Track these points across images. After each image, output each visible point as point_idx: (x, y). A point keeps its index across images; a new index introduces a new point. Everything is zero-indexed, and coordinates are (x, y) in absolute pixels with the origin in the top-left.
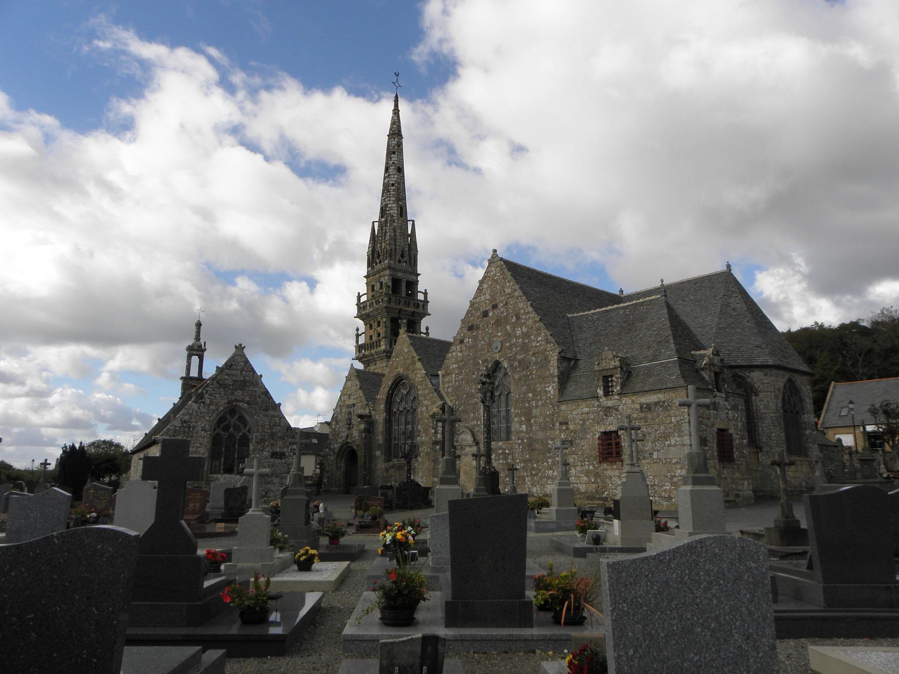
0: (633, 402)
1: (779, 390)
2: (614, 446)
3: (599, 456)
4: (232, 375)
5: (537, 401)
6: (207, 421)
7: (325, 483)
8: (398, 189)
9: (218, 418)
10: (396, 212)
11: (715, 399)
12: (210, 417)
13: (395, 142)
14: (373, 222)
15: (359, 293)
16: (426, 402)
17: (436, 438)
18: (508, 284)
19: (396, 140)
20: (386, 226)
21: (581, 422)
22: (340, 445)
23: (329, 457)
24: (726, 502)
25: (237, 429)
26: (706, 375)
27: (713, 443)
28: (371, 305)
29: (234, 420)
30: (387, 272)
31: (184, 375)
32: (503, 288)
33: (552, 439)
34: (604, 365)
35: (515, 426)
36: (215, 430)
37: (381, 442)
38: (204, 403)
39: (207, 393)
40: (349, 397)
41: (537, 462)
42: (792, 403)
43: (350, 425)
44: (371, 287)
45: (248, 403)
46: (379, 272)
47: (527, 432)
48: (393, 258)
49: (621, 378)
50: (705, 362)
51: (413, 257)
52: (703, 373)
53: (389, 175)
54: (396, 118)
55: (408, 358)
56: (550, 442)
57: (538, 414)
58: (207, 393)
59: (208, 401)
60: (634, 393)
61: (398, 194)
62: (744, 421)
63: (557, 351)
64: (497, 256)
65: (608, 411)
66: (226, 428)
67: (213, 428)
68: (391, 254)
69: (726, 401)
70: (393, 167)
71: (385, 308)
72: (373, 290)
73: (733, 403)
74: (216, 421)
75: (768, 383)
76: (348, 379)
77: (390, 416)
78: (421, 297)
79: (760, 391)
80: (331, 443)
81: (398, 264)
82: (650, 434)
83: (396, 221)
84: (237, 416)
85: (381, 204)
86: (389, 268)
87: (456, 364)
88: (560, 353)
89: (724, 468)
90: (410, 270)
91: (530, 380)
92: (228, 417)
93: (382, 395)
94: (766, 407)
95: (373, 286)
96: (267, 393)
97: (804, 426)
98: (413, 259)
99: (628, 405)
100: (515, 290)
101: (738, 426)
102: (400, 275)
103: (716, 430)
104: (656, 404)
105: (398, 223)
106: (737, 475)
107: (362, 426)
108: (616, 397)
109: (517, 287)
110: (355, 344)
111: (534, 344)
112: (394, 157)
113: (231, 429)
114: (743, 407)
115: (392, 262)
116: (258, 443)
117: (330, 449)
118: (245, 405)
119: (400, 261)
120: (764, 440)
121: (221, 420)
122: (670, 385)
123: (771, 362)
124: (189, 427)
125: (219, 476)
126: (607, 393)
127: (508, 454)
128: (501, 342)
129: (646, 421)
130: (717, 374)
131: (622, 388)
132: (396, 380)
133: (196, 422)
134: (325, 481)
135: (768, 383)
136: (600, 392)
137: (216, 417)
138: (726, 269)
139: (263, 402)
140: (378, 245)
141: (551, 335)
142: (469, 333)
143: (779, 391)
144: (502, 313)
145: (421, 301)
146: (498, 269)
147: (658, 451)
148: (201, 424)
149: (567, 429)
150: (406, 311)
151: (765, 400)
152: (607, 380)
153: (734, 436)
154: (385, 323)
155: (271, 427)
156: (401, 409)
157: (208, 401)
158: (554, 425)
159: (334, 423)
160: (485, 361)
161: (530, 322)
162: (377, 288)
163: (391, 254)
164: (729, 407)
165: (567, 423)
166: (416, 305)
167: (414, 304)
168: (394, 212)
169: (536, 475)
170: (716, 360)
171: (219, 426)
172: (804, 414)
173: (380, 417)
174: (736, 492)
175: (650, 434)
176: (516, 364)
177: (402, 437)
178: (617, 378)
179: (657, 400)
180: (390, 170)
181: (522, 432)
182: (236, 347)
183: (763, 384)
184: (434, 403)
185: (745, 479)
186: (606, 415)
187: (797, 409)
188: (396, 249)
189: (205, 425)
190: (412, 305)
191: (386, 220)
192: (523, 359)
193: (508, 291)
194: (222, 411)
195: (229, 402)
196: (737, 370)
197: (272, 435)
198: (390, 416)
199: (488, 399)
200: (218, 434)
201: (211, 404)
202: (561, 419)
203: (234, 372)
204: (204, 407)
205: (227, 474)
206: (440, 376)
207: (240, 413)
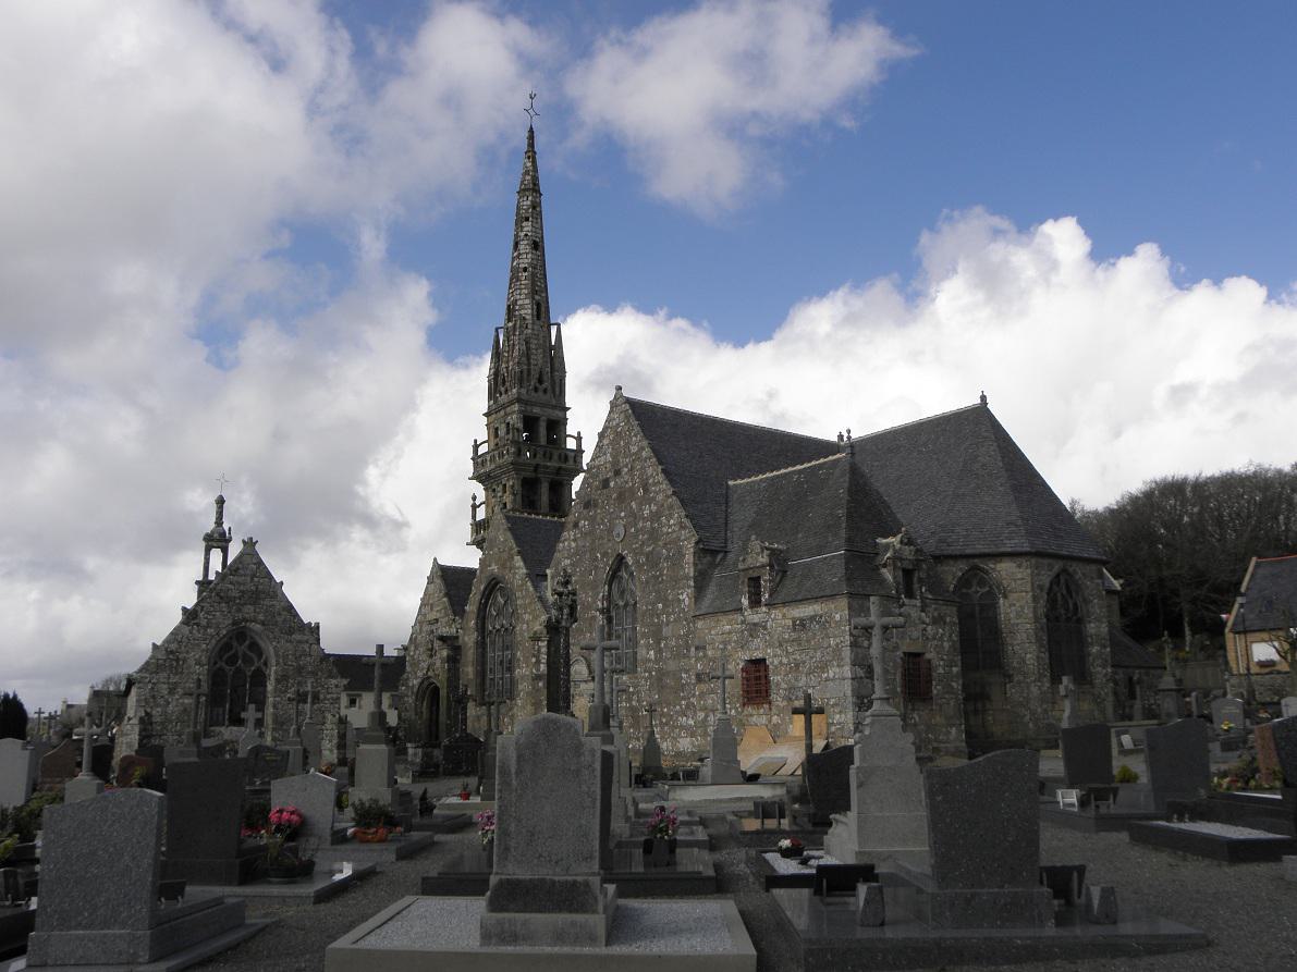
0: (784, 616)
1: (1041, 588)
2: (763, 678)
3: (743, 695)
4: (239, 584)
5: (668, 615)
6: (203, 651)
7: (400, 739)
8: (533, 275)
9: (220, 645)
10: (530, 311)
11: (902, 610)
12: (207, 645)
13: (529, 203)
14: (497, 329)
15: (476, 441)
16: (526, 617)
17: (538, 670)
18: (634, 439)
19: (530, 198)
20: (514, 335)
21: (721, 646)
22: (419, 680)
23: (406, 699)
24: (918, 759)
25: (248, 661)
26: (887, 574)
27: (895, 674)
28: (493, 459)
29: (243, 648)
30: (516, 407)
31: (201, 579)
32: (627, 445)
33: (687, 672)
34: (750, 562)
35: (641, 652)
36: (215, 663)
37: (471, 676)
38: (198, 625)
39: (202, 610)
40: (432, 609)
41: (668, 705)
42: (1071, 606)
43: (431, 652)
44: (493, 430)
45: (263, 624)
46: (504, 407)
47: (657, 661)
48: (525, 384)
49: (770, 581)
50: (888, 555)
51: (557, 381)
52: (884, 570)
53: (520, 254)
54: (529, 164)
55: (504, 551)
56: (683, 675)
57: (670, 634)
58: (202, 610)
59: (204, 622)
60: (784, 604)
61: (533, 283)
62: (955, 639)
63: (694, 540)
64: (622, 396)
65: (754, 629)
66: (232, 661)
67: (212, 661)
68: (521, 380)
69: (922, 611)
70: (526, 242)
71: (512, 464)
72: (496, 435)
73: (936, 614)
74: (217, 649)
75: (1023, 579)
76: (431, 580)
77: (483, 638)
78: (571, 444)
79: (1010, 591)
80: (408, 679)
81: (533, 394)
82: (804, 662)
83: (530, 326)
84: (247, 642)
85: (509, 299)
86: (519, 400)
87: (568, 558)
88: (697, 543)
89: (913, 710)
90: (554, 402)
91: (660, 583)
92: (235, 644)
93: (471, 608)
94: (1019, 616)
95: (497, 429)
96: (290, 608)
97: (1090, 640)
98: (557, 385)
99: (779, 619)
100: (643, 449)
101: (943, 648)
102: (536, 410)
103: (902, 655)
104: (812, 618)
105: (533, 329)
106: (938, 719)
107: (445, 653)
108: (764, 609)
109: (645, 443)
110: (470, 521)
111: (665, 530)
112: (527, 226)
113: (240, 662)
114: (956, 620)
115: (523, 391)
116: (278, 681)
117: (408, 687)
118: (258, 626)
119: (536, 390)
120: (1015, 664)
121: (226, 647)
122: (828, 592)
123: (1026, 548)
124: (177, 660)
125: (222, 729)
126: (755, 602)
127: (633, 693)
128: (624, 526)
129: (800, 644)
130: (908, 573)
131: (770, 596)
132: (490, 583)
133: (187, 652)
134: (400, 734)
135: (1023, 579)
136: (745, 602)
137: (216, 644)
138: (979, 401)
139: (285, 620)
140: (504, 366)
141: (687, 516)
142: (585, 512)
143: (1042, 590)
144: (627, 482)
145: (572, 450)
146: (622, 415)
147: (814, 687)
148: (194, 655)
149: (705, 656)
150: (548, 467)
151: (1018, 605)
152: (755, 582)
153: (935, 662)
154: (512, 487)
155: (297, 658)
156: (498, 627)
157: (204, 622)
158: (688, 651)
159: (413, 648)
160: (605, 554)
161: (660, 497)
162: (502, 432)
163: (521, 380)
164: (927, 620)
165: (704, 648)
166: (563, 457)
167: (560, 456)
168: (527, 312)
169: (666, 724)
170: (908, 552)
171: (221, 658)
172: (1090, 622)
173: (469, 639)
174: (935, 745)
175: (804, 662)
176: (643, 559)
177: (498, 667)
178: (765, 581)
179: (812, 613)
180: (521, 247)
181: (650, 660)
182: (244, 542)
183: (1015, 580)
184: (536, 618)
185: (952, 725)
186: (751, 636)
187: (1079, 615)
188: (529, 370)
189: (200, 657)
190: (555, 457)
191: (515, 325)
192: (651, 552)
193: (634, 449)
194: (224, 636)
195: (234, 623)
196: (976, 560)
197: (300, 670)
198: (483, 638)
199: (565, 617)
200: (221, 669)
201: (208, 626)
202: (697, 643)
203: (241, 579)
204: (199, 631)
205: (235, 725)
206: (549, 577)
207: (252, 638)
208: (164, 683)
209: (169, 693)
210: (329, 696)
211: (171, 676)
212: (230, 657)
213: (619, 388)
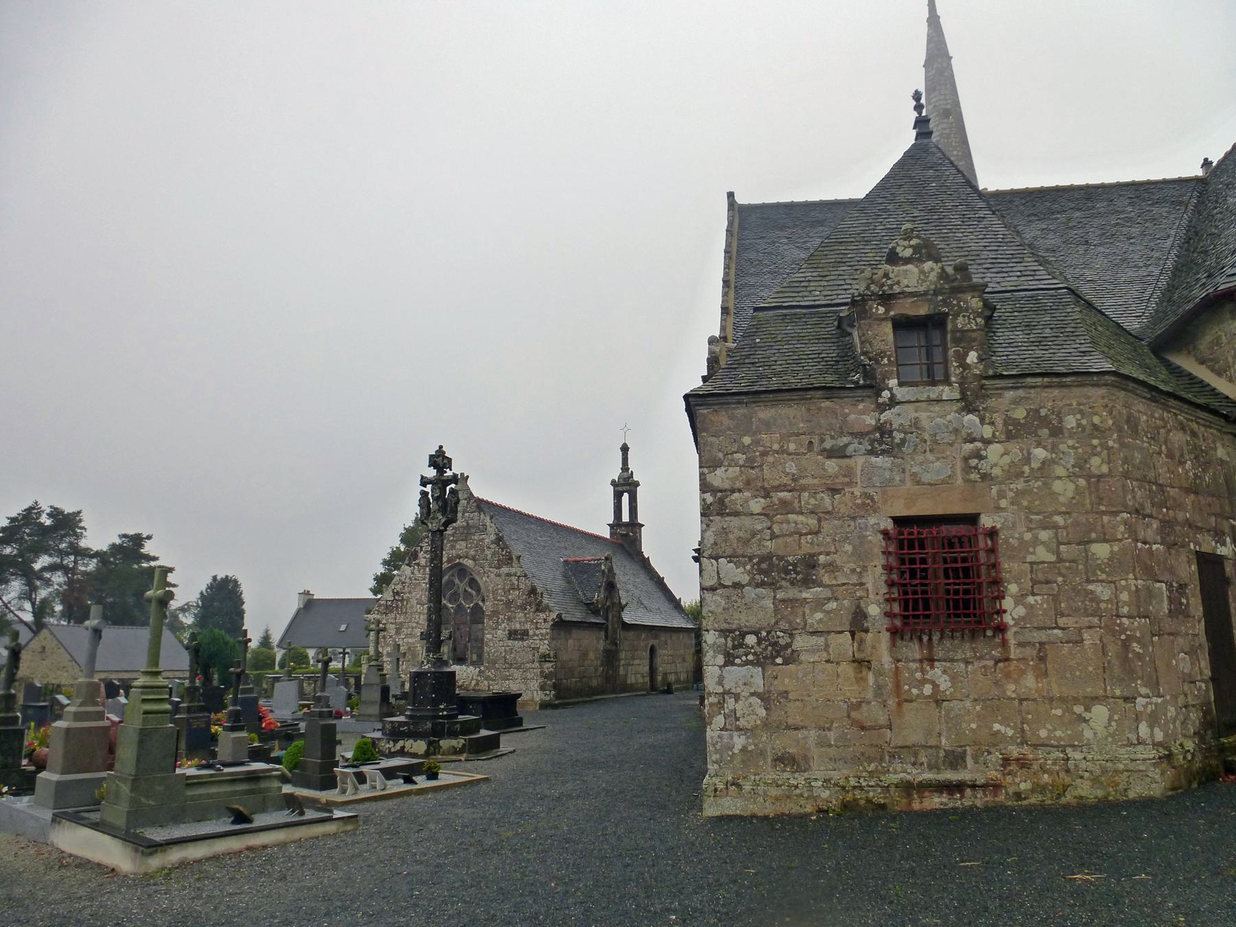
38: (418, 564)
45: (474, 559)
92: (457, 581)
103: (889, 525)
118: (470, 561)
189: (421, 596)
204: (419, 571)
208: (391, 623)
209: (396, 633)
210: (537, 632)
211: (398, 616)
212: (452, 595)
213: (731, 195)
